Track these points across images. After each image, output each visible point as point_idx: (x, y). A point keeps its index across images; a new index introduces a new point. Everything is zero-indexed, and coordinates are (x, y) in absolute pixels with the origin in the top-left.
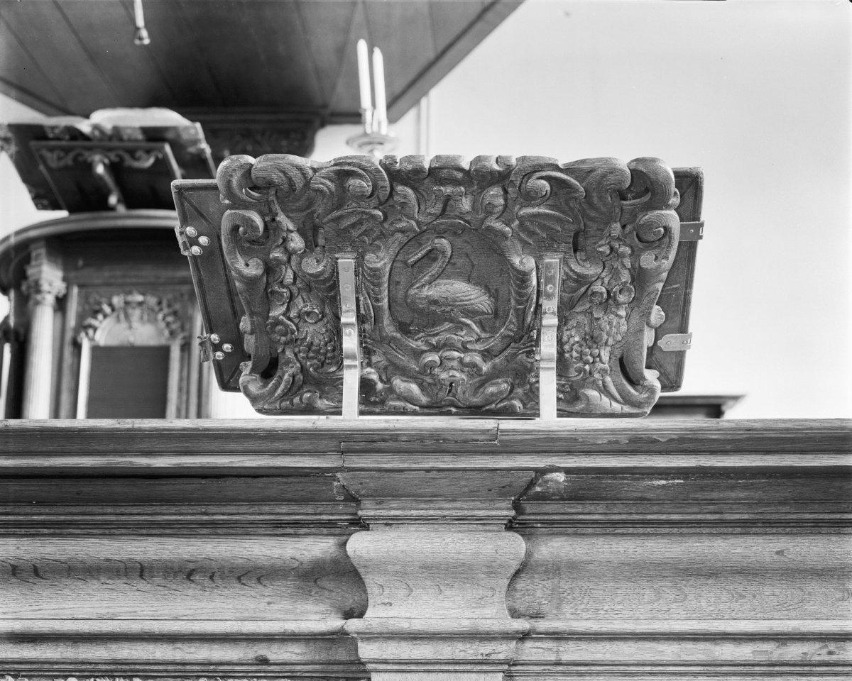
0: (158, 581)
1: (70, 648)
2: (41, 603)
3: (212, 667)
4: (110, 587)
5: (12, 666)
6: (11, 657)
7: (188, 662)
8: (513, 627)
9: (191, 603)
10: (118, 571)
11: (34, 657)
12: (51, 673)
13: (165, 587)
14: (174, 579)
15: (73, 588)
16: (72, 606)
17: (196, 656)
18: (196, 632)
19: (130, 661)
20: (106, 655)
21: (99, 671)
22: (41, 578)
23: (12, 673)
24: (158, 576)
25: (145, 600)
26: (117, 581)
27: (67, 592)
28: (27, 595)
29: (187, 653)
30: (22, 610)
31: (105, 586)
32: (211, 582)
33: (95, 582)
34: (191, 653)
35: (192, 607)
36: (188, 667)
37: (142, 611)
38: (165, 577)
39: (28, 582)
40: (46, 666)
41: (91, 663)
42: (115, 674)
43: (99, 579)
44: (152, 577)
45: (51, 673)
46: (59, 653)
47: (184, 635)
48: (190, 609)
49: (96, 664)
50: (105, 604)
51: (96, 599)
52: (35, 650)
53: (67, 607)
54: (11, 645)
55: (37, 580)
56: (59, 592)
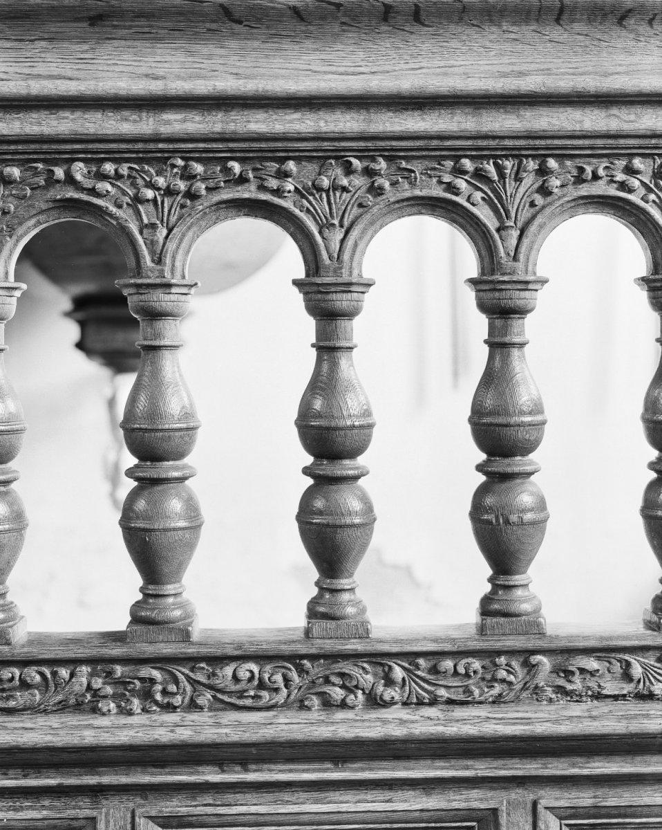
0: (577, 27)
1: (469, 117)
2: (420, 59)
3: (653, 141)
4: (513, 36)
5: (388, 143)
6: (391, 129)
7: (625, 133)
8: (86, 741)
9: (622, 57)
10: (529, 12)
11: (422, 129)
12: (438, 153)
13: (587, 35)
14: (601, 23)
15: (464, 38)
16: (462, 63)
17: (637, 125)
18: (644, 91)
19: (551, 133)
20: (519, 125)
21: (502, 149)
22: (424, 25)
23: (387, 154)
24: (579, 21)
25: (560, 54)
26: (523, 27)
27: (454, 44)
28: (400, 48)
29: (625, 121)
30: (397, 68)
31: (506, 36)
32: (648, 28)
33: (494, 29)
34: (632, 122)
35: (623, 62)
36: (622, 141)
37: (558, 69)
38: (590, 21)
39: (404, 30)
40: (435, 143)
41: (494, 138)
42: (524, 152)
43: (500, 26)
44: (573, 21)
45: (438, 153)
46: (455, 124)
47: (628, 95)
48: (620, 65)
49: (503, 138)
50: (506, 60)
51: (493, 53)
52: (423, 119)
53: (455, 63)
54: (391, 114)
55: (417, 28)
56: (445, 44)
